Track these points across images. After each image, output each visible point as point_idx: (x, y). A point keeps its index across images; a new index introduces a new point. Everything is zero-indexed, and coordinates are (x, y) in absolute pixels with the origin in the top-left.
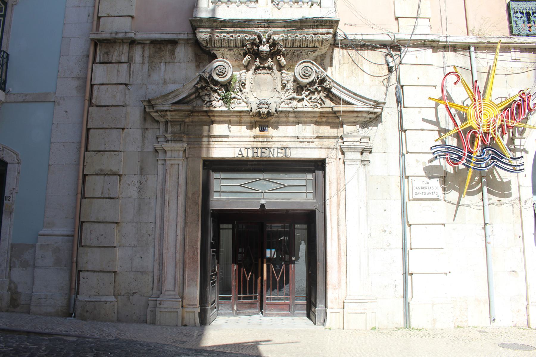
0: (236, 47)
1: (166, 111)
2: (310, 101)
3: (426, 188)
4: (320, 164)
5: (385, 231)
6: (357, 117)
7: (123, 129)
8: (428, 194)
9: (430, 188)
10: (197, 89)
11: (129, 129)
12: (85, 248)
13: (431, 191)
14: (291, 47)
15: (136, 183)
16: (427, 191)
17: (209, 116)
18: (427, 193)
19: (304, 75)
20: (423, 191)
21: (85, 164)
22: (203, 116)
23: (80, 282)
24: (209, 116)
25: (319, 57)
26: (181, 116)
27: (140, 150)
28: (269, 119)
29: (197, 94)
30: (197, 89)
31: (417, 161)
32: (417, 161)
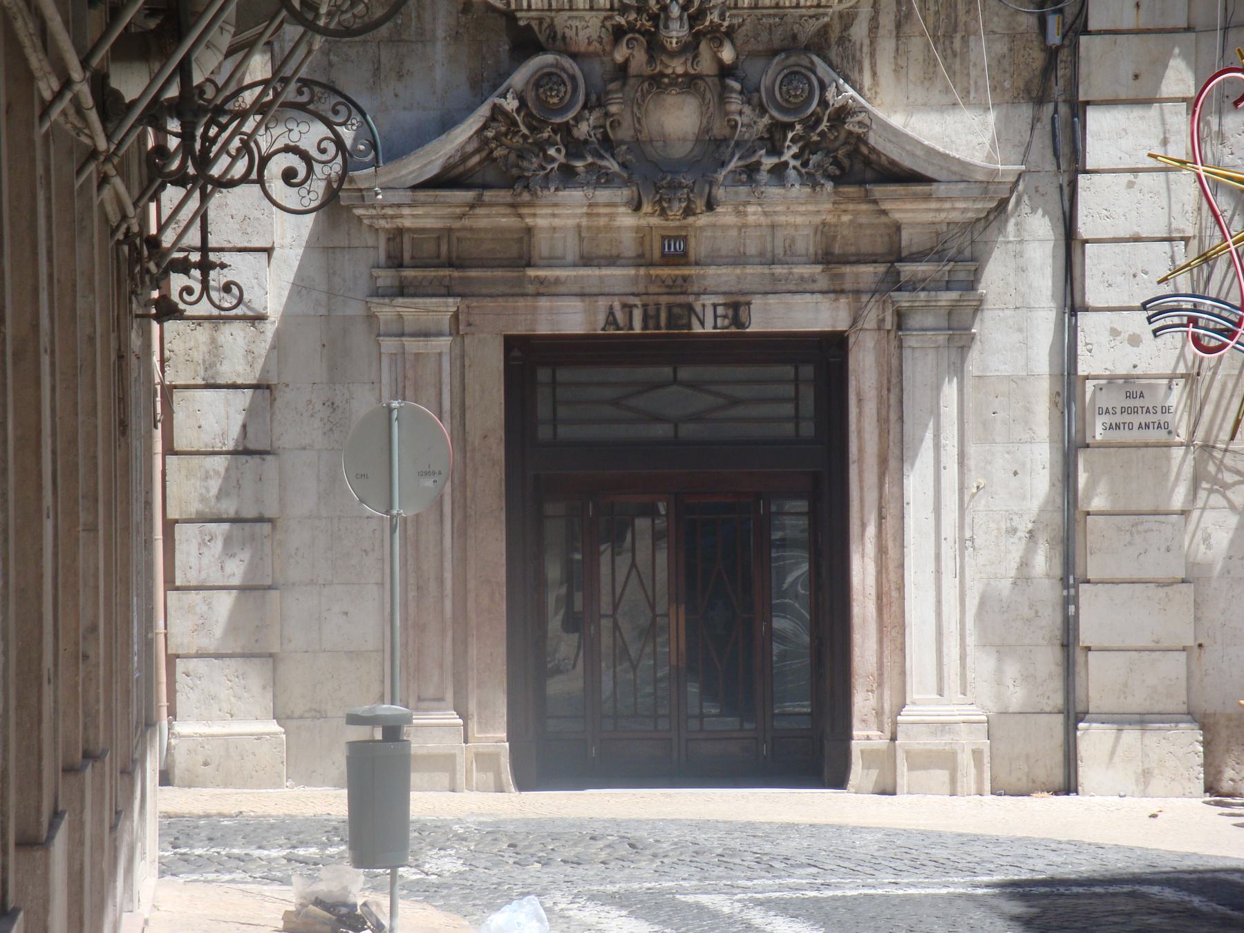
0: (591, 9)
1: (399, 206)
2: (803, 171)
3: (1134, 411)
4: (516, 353)
5: (1015, 530)
6: (939, 210)
7: (268, 251)
8: (1140, 427)
9: (1148, 411)
10: (486, 142)
11: (287, 251)
12: (1096, 177)
13: (1150, 418)
14: (750, 8)
15: (319, 406)
16: (1137, 419)
17: (520, 216)
18: (1136, 426)
19: (787, 101)
20: (1127, 418)
21: (167, 354)
22: (504, 215)
23: (178, 686)
24: (520, 216)
25: (836, 20)
26: (442, 217)
27: (322, 311)
28: (691, 219)
29: (484, 154)
30: (486, 142)
31: (1115, 333)
32: (1115, 333)
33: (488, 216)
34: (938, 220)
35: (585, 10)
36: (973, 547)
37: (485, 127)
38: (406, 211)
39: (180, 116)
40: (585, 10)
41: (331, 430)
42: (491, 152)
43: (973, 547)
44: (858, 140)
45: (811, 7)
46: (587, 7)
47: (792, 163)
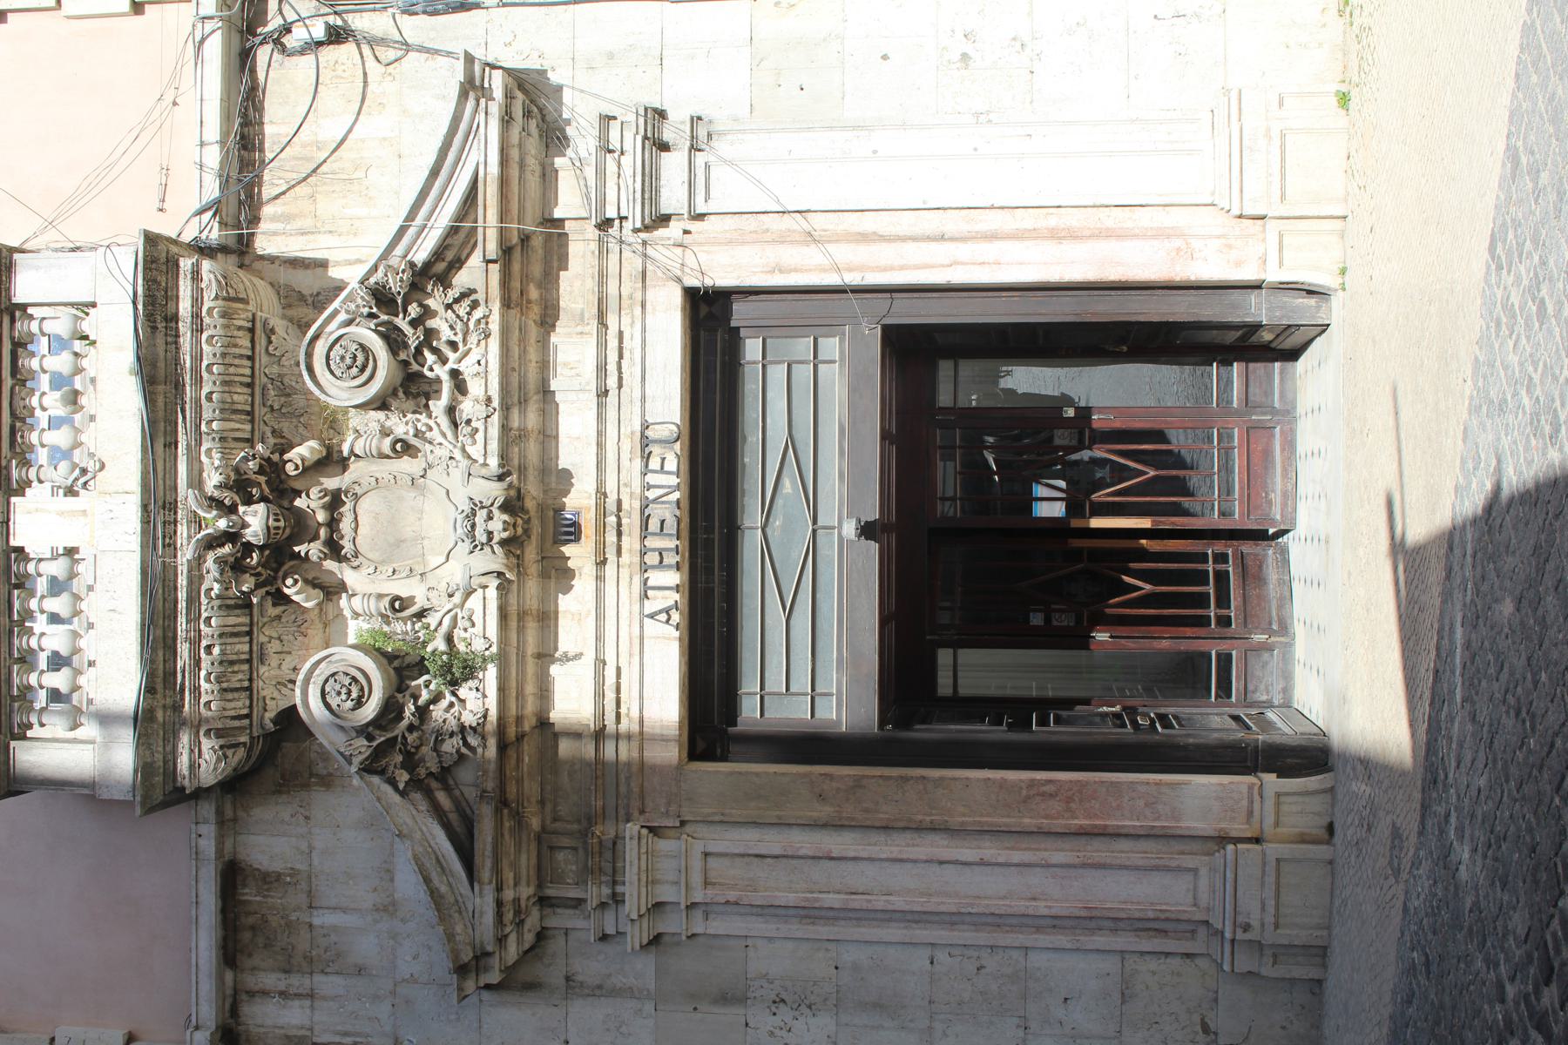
0: (250, 633)
1: (499, 903)
14: (252, 422)
17: (520, 737)
19: (362, 370)
24: (520, 737)
25: (290, 312)
26: (518, 846)
27: (649, 1007)
28: (530, 504)
29: (434, 784)
30: (416, 783)
33: (519, 781)
34: (538, 169)
35: (251, 642)
36: (988, 112)
37: (392, 782)
38: (509, 894)
39: (1042, 472)
40: (251, 642)
41: (810, 1007)
42: (431, 774)
43: (988, 112)
44: (1475, 521)
45: (253, 341)
46: (247, 639)
47: (450, 365)
